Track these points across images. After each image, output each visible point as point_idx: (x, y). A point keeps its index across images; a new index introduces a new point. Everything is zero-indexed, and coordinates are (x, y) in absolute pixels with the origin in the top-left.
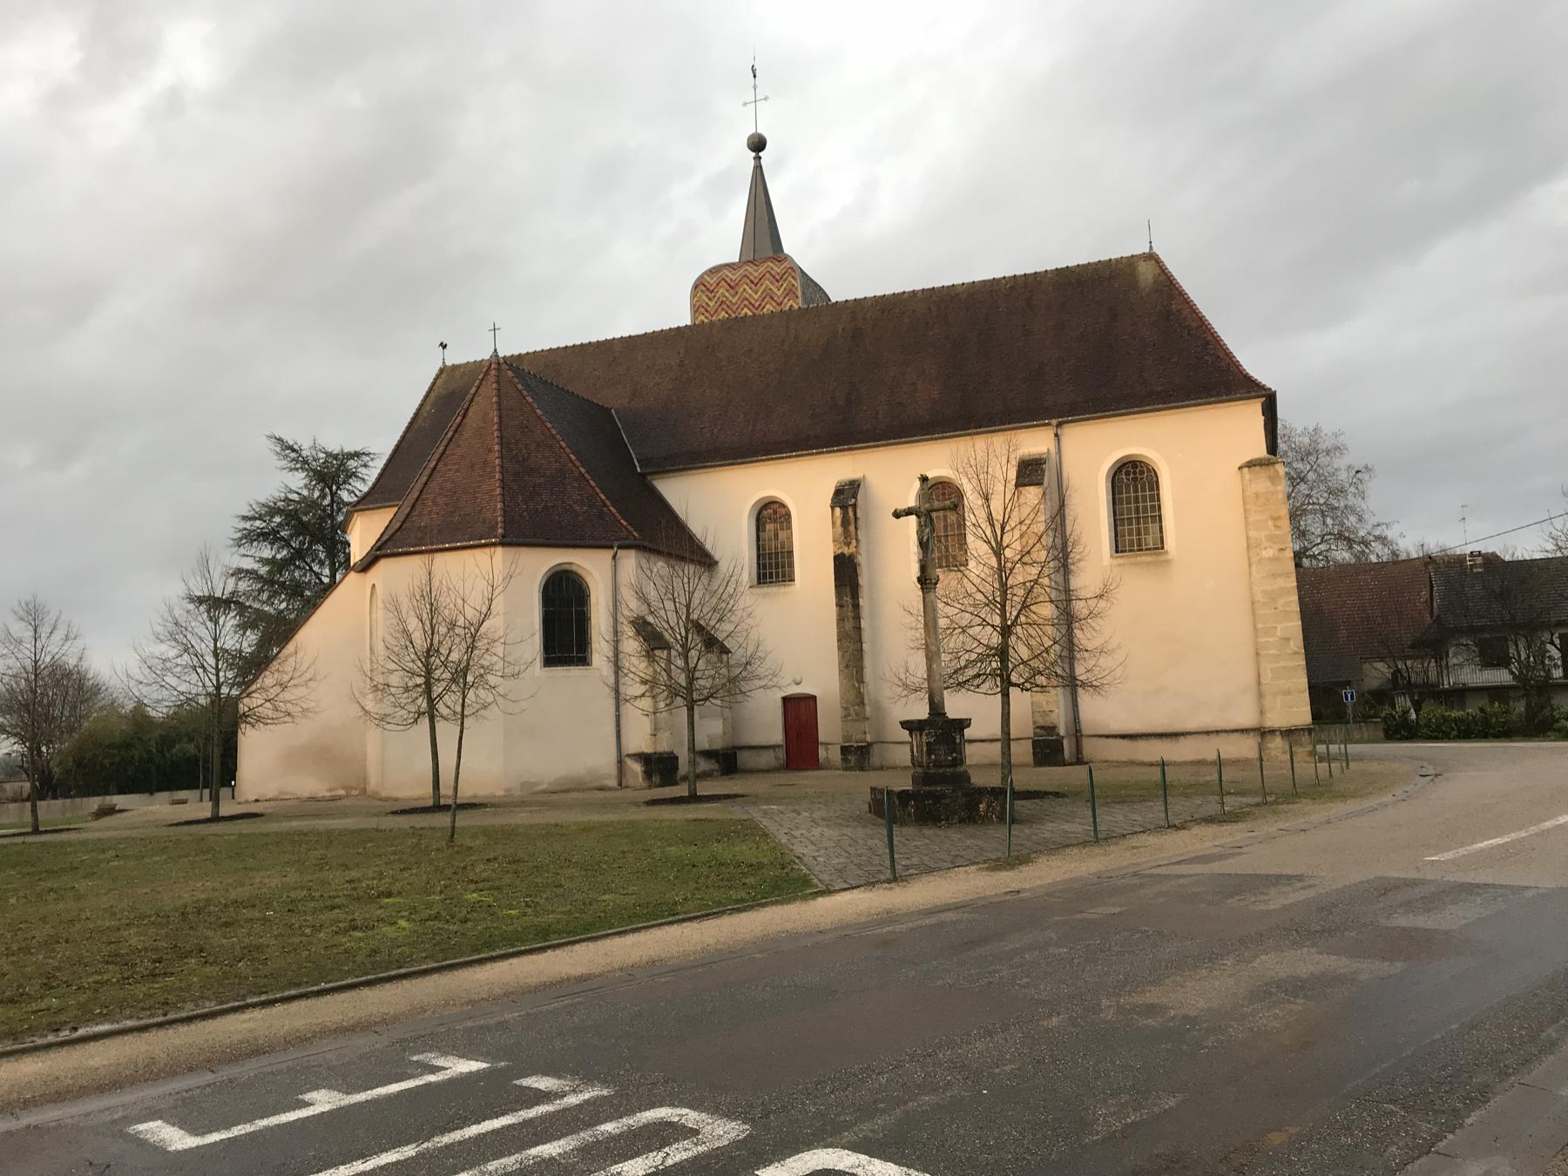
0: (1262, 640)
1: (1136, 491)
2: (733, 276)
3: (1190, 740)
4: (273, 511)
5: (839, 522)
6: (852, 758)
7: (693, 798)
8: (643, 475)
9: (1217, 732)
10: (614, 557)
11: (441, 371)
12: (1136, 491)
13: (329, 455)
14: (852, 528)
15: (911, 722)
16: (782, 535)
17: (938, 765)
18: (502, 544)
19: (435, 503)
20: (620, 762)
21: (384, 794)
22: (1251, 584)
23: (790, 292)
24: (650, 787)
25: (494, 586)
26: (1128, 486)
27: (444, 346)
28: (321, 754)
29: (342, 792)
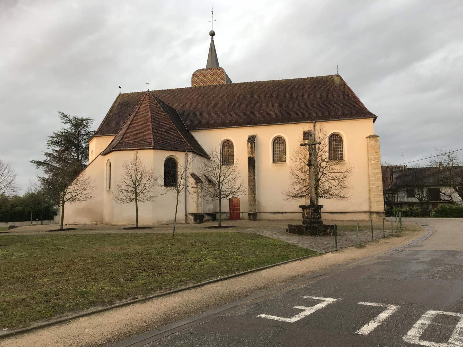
0: (371, 186)
1: (336, 143)
2: (205, 73)
3: (349, 214)
4: (58, 136)
5: (250, 148)
6: (252, 217)
7: (220, 227)
8: (188, 130)
9: (357, 212)
10: (186, 154)
11: (120, 95)
12: (336, 143)
13: (78, 119)
14: (253, 149)
15: (302, 206)
16: (230, 150)
17: (314, 218)
18: (154, 149)
19: (131, 135)
20: (186, 216)
21: (113, 223)
22: (368, 171)
23: (222, 79)
24: (196, 223)
25: (151, 161)
26: (333, 141)
27: (120, 88)
28: (88, 211)
29: (95, 223)
